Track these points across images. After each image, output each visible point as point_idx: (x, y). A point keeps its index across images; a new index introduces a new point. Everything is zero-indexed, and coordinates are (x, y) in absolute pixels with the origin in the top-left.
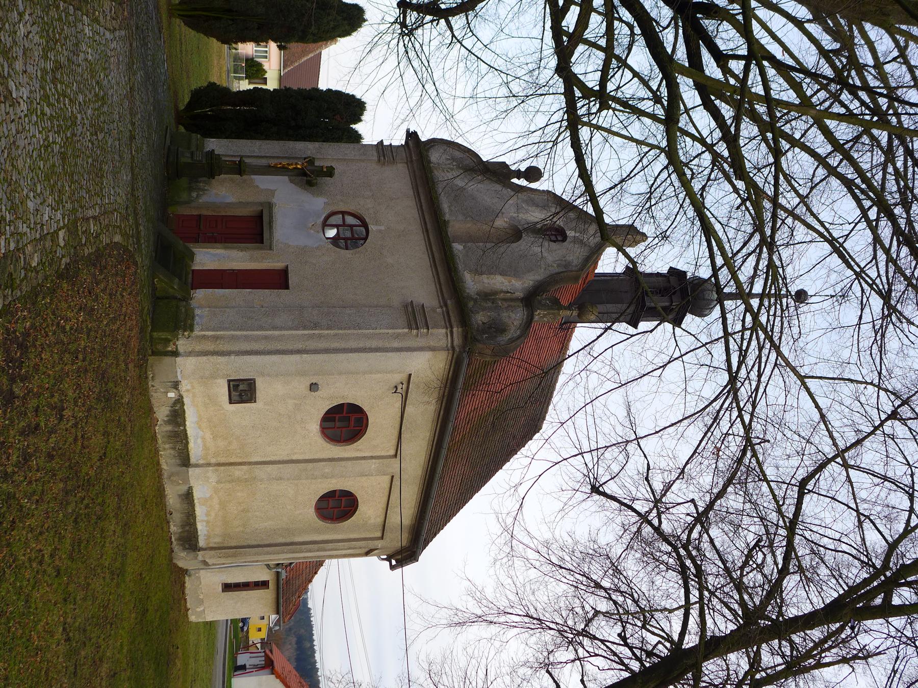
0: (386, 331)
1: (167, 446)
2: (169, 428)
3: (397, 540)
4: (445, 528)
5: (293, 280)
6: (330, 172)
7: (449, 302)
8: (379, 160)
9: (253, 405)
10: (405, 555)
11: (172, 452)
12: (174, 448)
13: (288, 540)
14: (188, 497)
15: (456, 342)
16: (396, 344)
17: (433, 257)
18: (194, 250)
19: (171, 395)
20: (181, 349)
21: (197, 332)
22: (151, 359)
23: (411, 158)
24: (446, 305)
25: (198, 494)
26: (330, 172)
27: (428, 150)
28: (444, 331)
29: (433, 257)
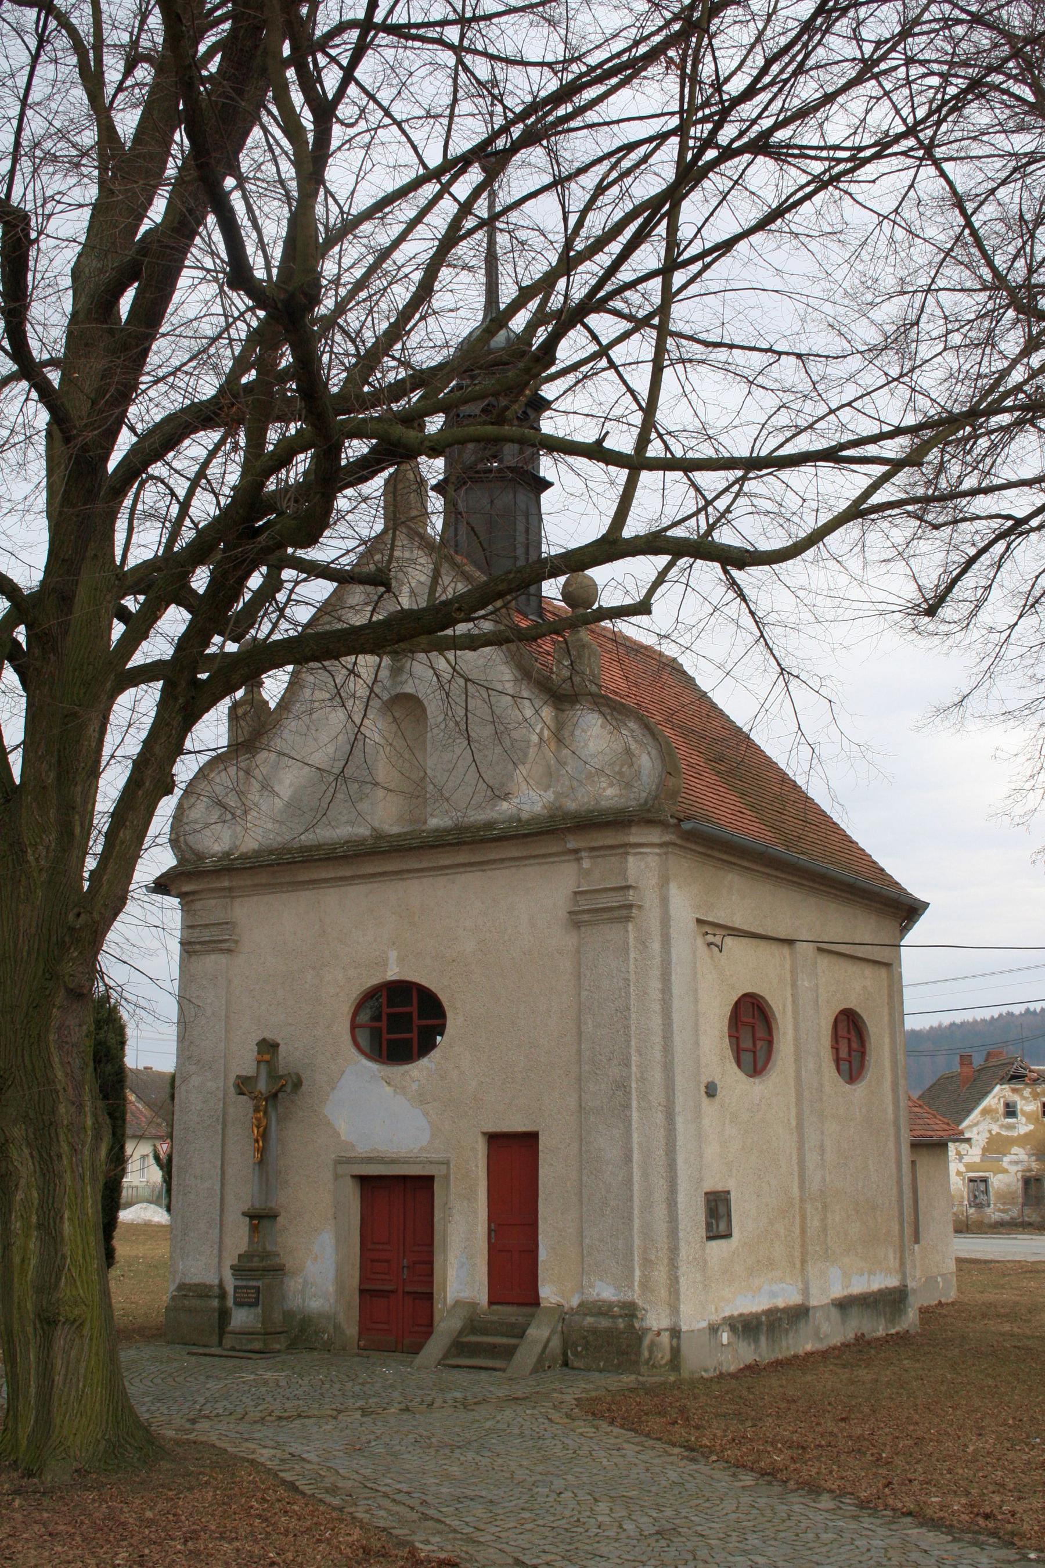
0: (632, 961)
1: (784, 1344)
2: (763, 1339)
3: (860, 928)
4: (855, 838)
5: (517, 1124)
6: (268, 1048)
7: (571, 846)
8: (229, 951)
9: (732, 1194)
10: (906, 910)
11: (791, 1335)
12: (787, 1331)
13: (892, 1131)
14: (844, 1305)
15: (656, 840)
16: (656, 946)
17: (464, 865)
18: (450, 1301)
19: (725, 1337)
20: (665, 1323)
21: (635, 1294)
22: (685, 1374)
23: (223, 889)
24: (576, 851)
25: (838, 1291)
26: (268, 1048)
27: (200, 857)
28: (631, 859)
29: (464, 865)
